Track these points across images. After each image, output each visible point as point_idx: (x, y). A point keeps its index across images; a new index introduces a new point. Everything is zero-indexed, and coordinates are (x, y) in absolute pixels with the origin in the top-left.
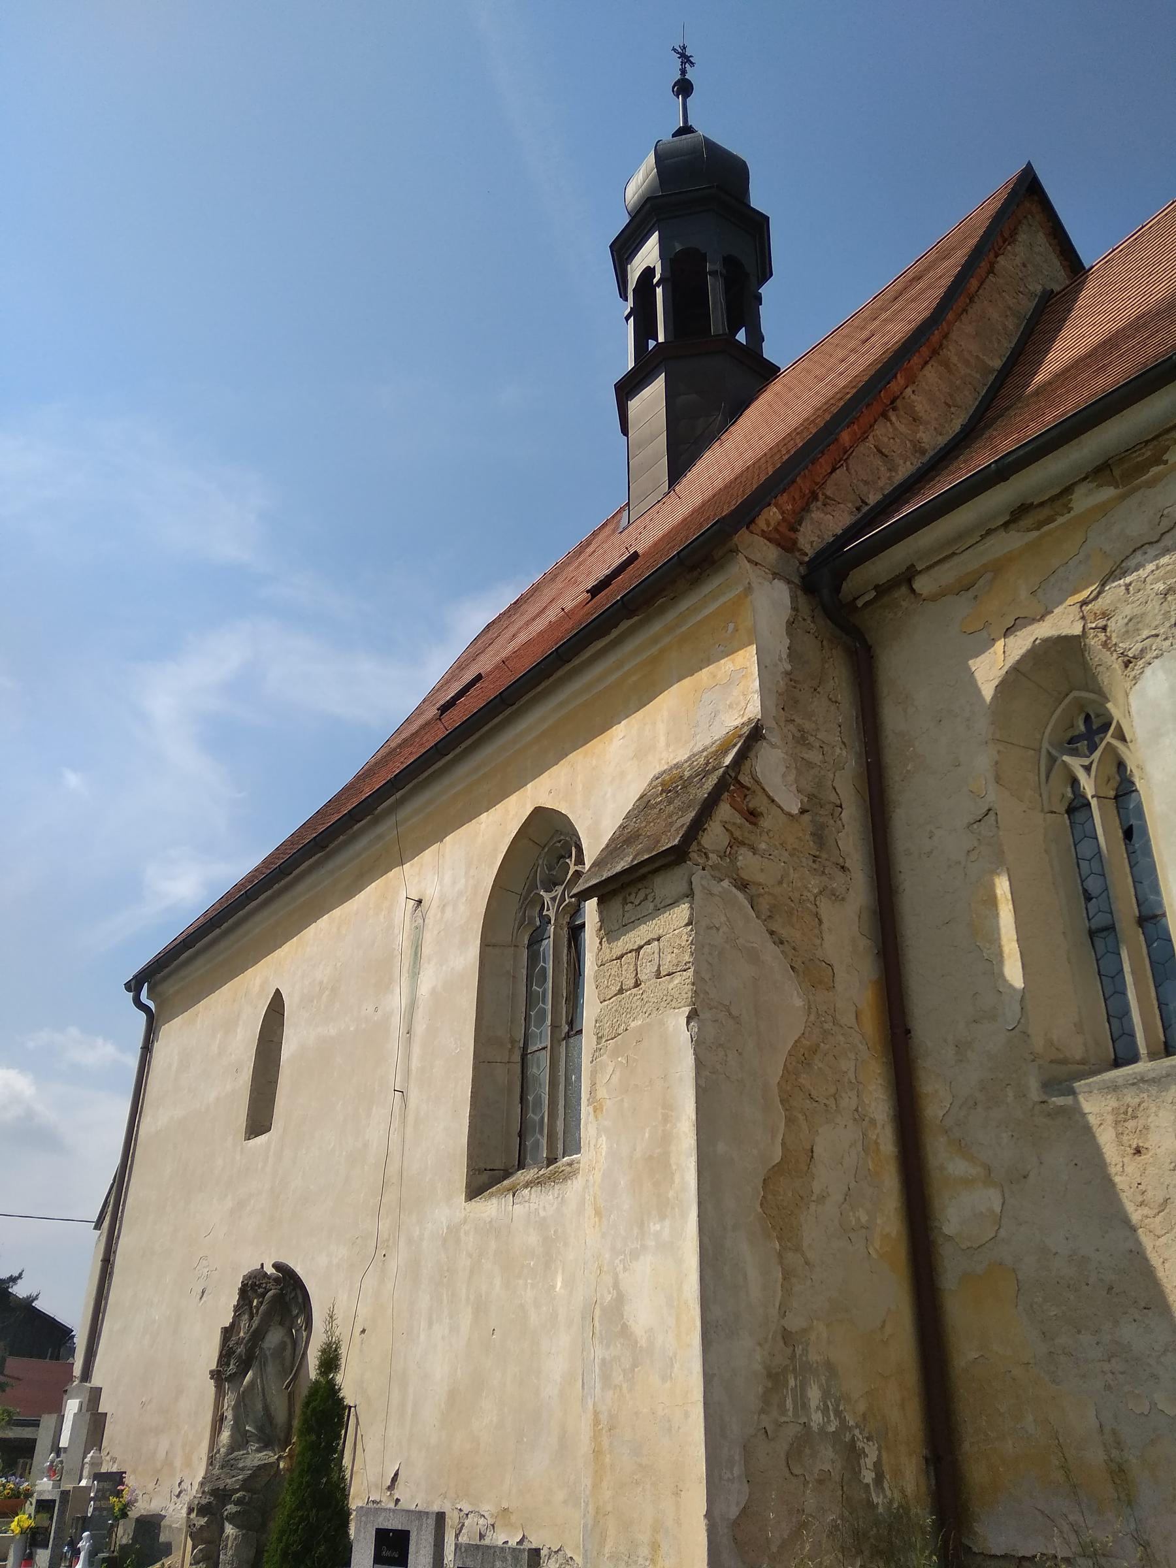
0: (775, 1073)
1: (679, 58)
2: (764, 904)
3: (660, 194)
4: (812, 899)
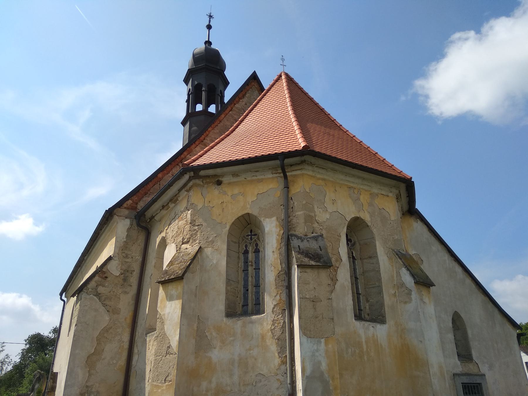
0: (97, 333)
1: (208, 17)
2: (103, 298)
3: (194, 67)
4: (119, 294)
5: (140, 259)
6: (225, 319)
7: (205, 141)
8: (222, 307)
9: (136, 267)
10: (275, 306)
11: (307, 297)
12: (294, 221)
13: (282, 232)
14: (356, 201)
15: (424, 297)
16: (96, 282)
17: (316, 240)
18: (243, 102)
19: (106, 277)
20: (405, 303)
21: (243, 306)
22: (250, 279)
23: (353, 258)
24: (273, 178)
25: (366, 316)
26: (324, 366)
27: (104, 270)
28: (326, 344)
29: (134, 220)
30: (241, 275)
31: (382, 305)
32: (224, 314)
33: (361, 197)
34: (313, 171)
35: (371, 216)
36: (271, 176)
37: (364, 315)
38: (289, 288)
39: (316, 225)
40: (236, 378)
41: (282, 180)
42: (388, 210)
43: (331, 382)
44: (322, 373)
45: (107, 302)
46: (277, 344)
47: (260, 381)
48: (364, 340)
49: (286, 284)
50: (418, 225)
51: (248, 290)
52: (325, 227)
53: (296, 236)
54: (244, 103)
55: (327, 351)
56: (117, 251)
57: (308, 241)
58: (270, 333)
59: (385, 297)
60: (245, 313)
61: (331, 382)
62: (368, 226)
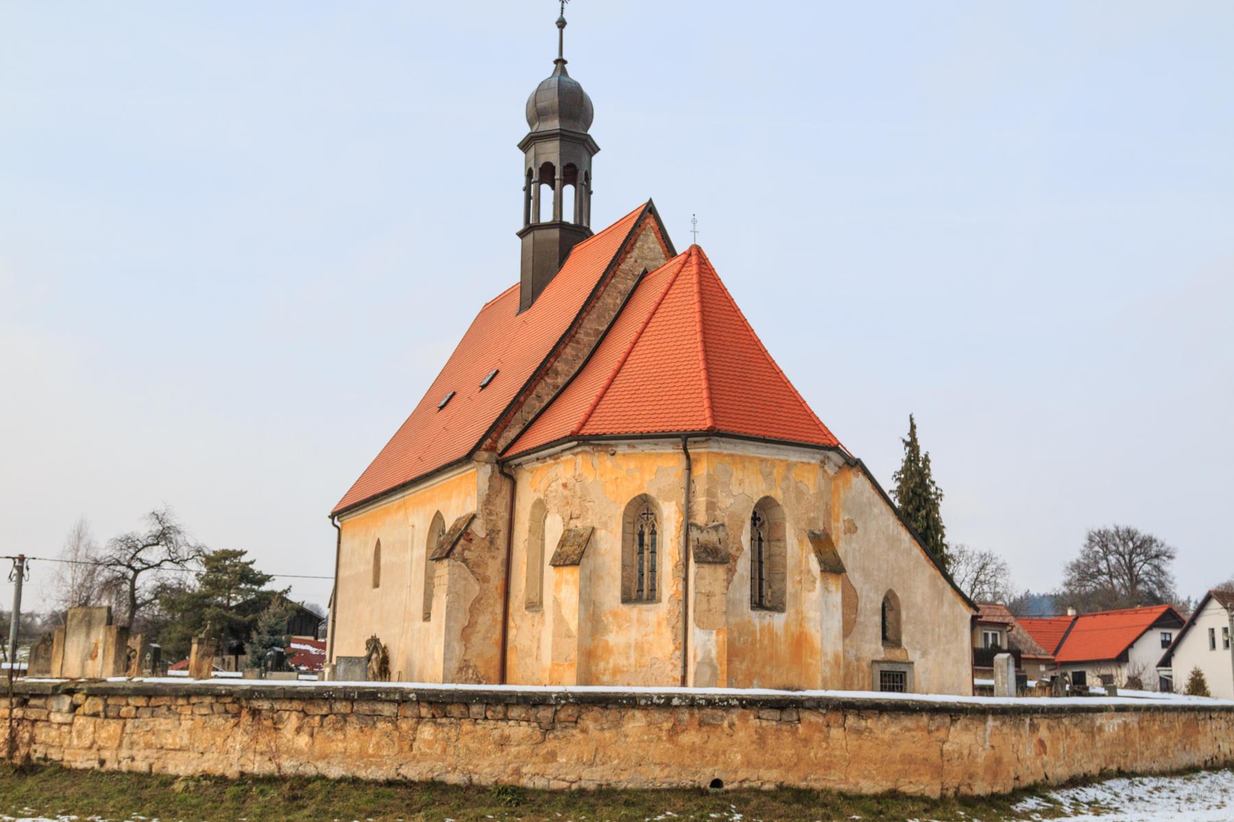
5: (506, 515)
6: (621, 605)
7: (577, 336)
8: (617, 592)
9: (502, 526)
10: (671, 596)
11: (703, 591)
12: (695, 507)
13: (682, 519)
14: (767, 476)
15: (830, 585)
16: (461, 546)
17: (717, 531)
18: (631, 257)
19: (471, 540)
20: (809, 591)
21: (638, 591)
22: (645, 564)
23: (760, 539)
24: (674, 454)
25: (767, 603)
26: (714, 654)
27: (469, 531)
28: (718, 634)
29: (496, 465)
30: (636, 558)
31: (784, 593)
32: (620, 600)
33: (775, 471)
34: (720, 448)
35: (784, 493)
36: (671, 451)
37: (766, 602)
38: (686, 579)
39: (718, 512)
40: (632, 661)
41: (683, 458)
42: (806, 482)
43: (719, 667)
44: (712, 660)
45: (476, 570)
46: (672, 631)
47: (655, 664)
48: (758, 629)
49: (683, 575)
50: (859, 481)
51: (643, 575)
52: (728, 513)
53: (696, 525)
54: (633, 260)
55: (717, 642)
56: (480, 508)
57: (708, 532)
58: (666, 622)
59: (788, 584)
60: (639, 600)
61: (719, 667)
62: (779, 505)
